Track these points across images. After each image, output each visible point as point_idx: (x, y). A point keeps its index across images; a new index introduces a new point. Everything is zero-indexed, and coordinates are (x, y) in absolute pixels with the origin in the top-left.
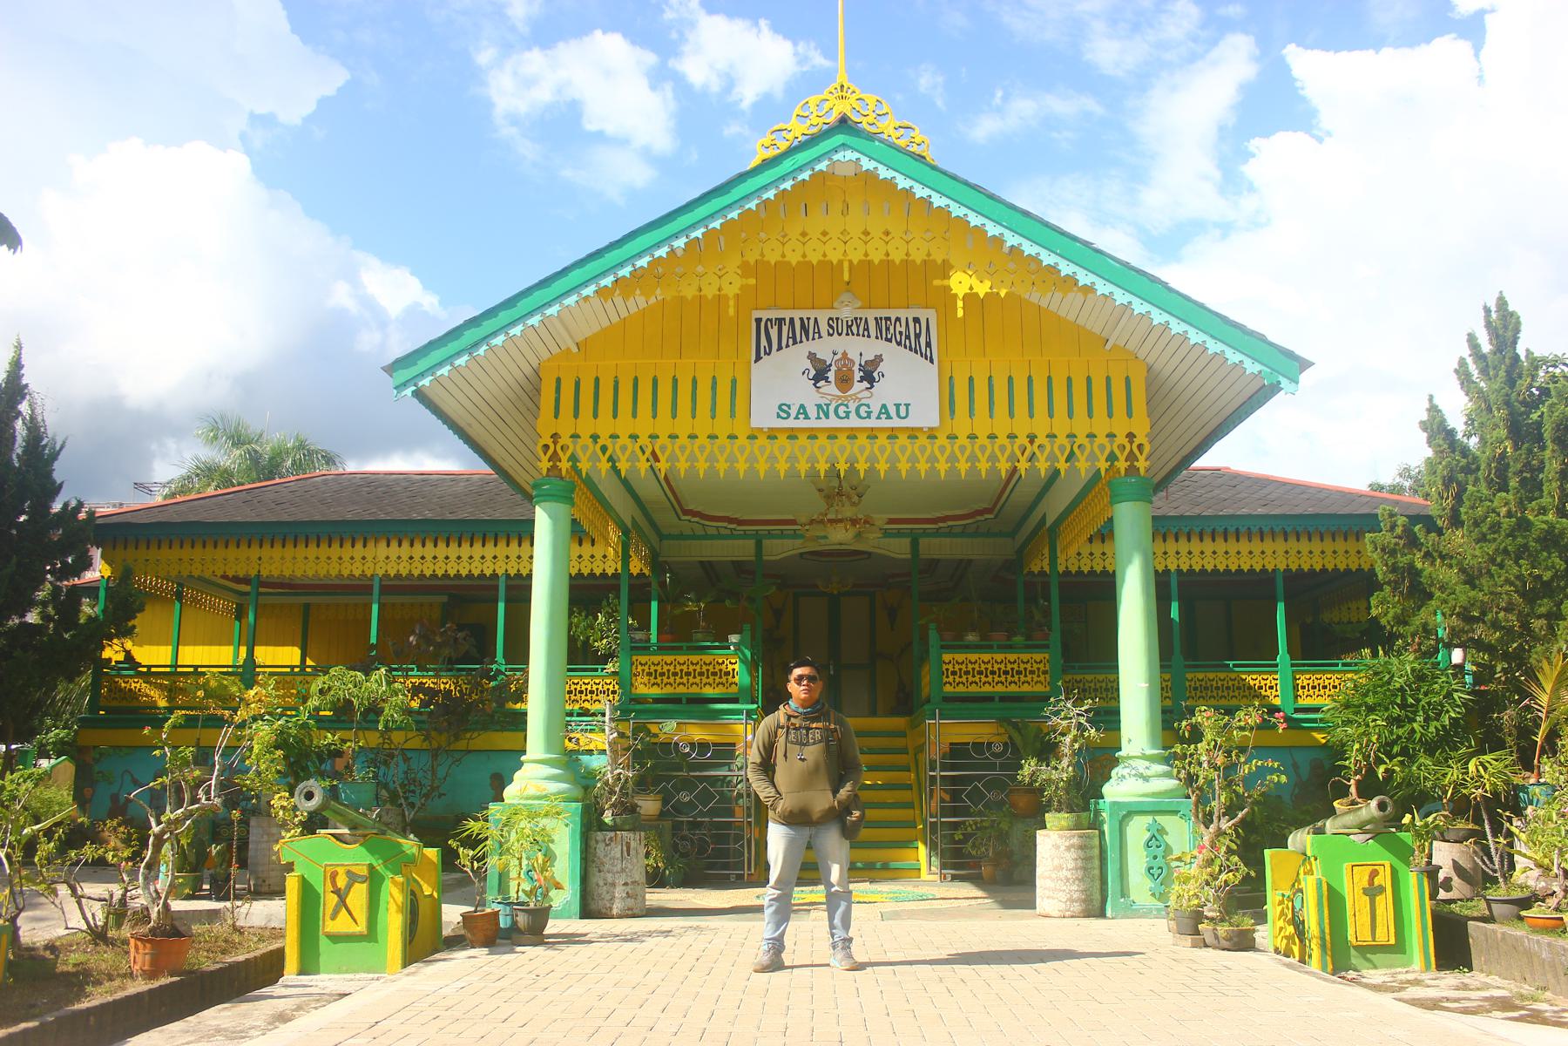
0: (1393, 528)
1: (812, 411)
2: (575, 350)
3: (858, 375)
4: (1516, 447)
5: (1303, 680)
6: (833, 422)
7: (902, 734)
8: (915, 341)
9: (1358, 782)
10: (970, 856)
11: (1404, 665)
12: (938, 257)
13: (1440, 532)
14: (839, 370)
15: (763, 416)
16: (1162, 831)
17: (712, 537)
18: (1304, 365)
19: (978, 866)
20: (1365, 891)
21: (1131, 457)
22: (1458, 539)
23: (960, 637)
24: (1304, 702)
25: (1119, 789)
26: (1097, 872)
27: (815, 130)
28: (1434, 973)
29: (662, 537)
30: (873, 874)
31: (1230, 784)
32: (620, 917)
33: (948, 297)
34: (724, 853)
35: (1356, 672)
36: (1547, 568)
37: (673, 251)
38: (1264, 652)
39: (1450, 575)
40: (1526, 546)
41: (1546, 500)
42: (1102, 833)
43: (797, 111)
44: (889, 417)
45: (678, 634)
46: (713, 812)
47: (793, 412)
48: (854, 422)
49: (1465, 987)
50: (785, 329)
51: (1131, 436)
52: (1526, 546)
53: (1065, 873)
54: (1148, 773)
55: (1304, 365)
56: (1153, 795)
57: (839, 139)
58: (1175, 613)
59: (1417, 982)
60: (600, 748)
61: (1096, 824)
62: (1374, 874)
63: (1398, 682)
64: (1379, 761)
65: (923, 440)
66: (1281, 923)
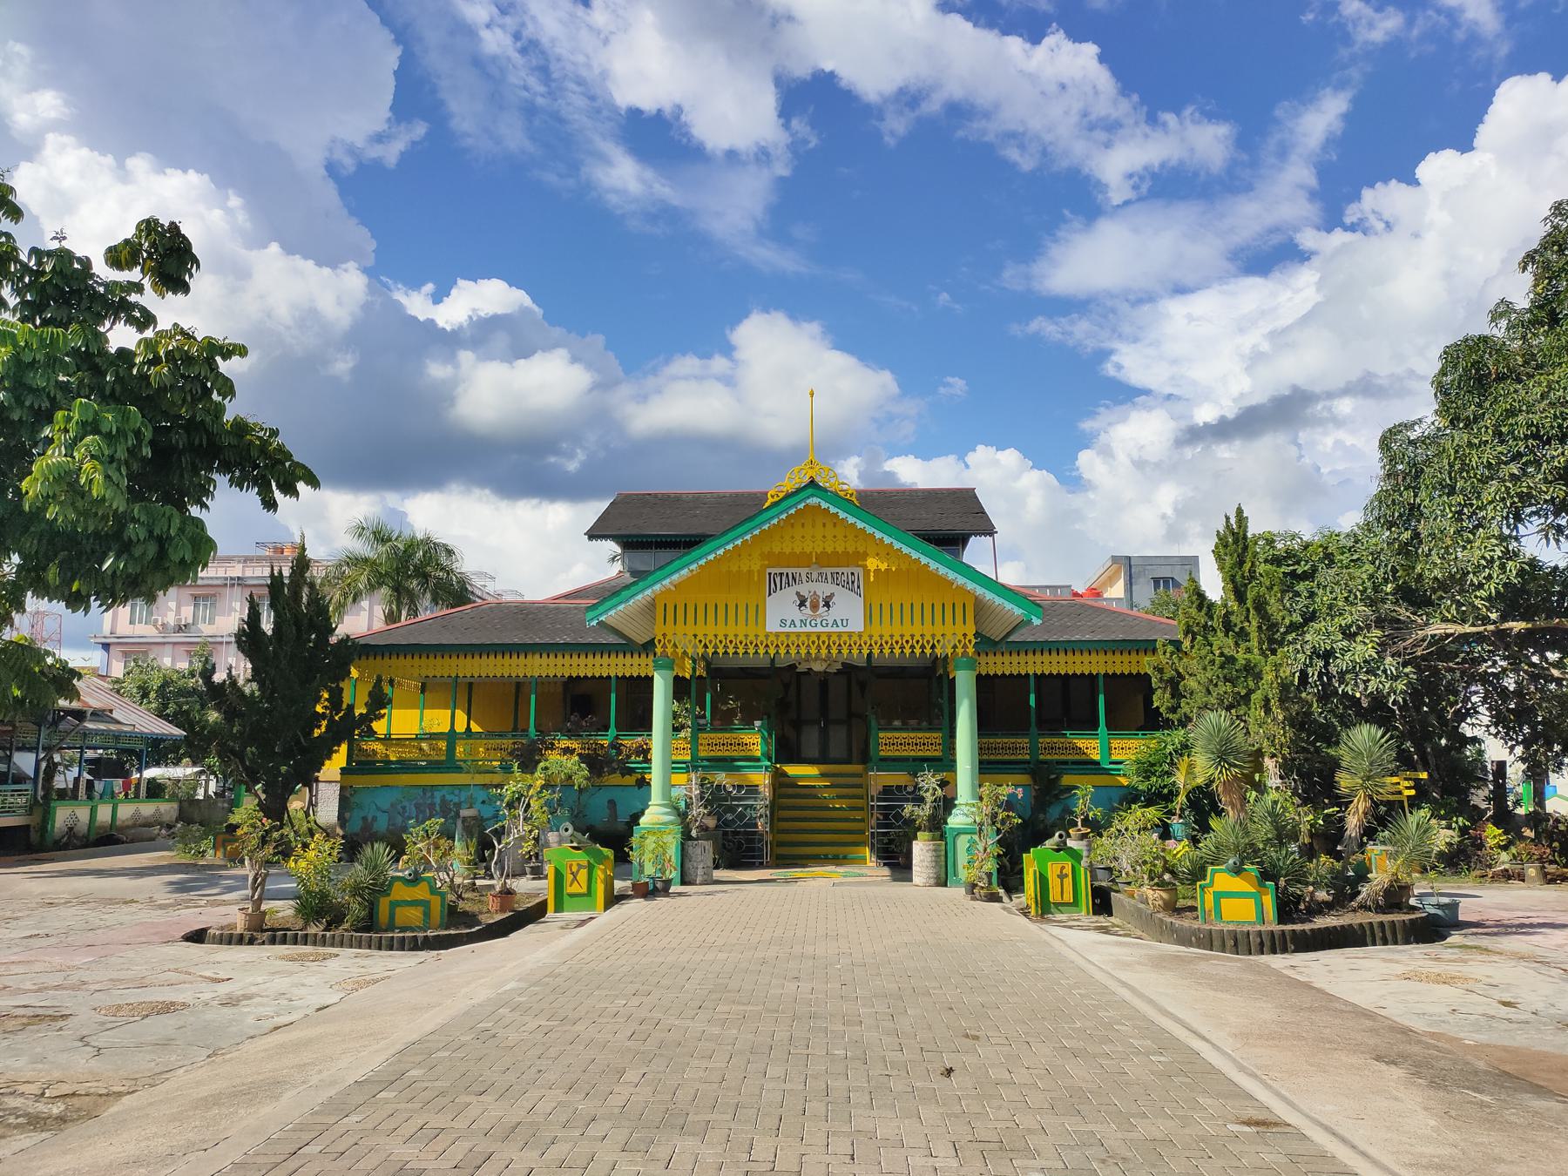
1: (798, 623)
5: (1115, 744)
6: (809, 629)
7: (860, 776)
8: (851, 586)
12: (861, 550)
15: (772, 626)
23: (890, 723)
24: (1114, 758)
25: (956, 820)
45: (723, 721)
48: (819, 629)
57: (810, 491)
60: (686, 786)
61: (942, 837)
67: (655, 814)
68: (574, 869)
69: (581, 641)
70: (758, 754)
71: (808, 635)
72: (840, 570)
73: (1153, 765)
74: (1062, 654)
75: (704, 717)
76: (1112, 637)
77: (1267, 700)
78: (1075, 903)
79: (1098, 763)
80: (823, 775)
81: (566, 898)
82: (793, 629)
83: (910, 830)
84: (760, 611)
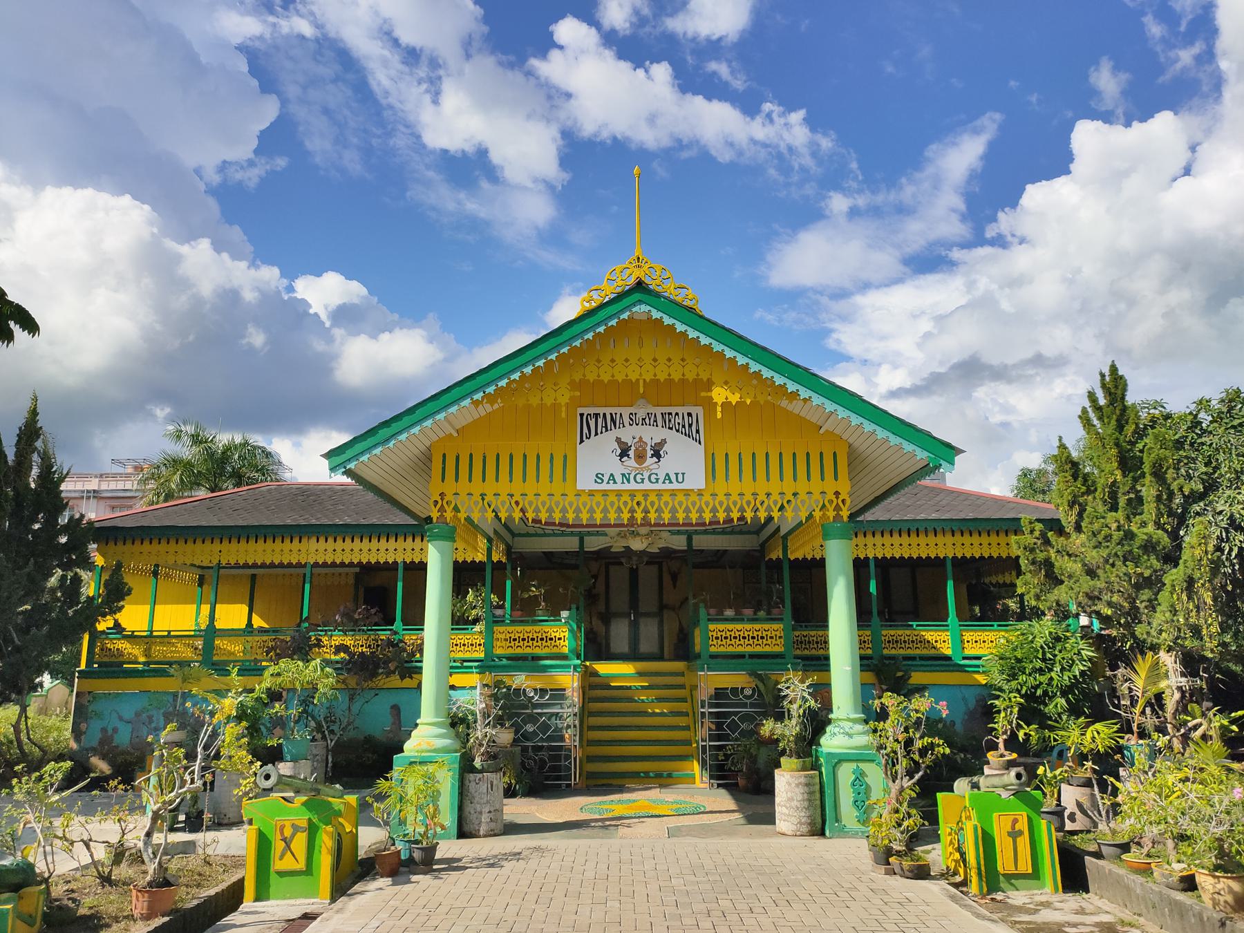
0: (1032, 532)
1: (619, 478)
2: (455, 434)
3: (650, 453)
4: (1124, 476)
5: (967, 636)
6: (633, 486)
8: (688, 429)
9: (1005, 741)
10: (730, 770)
11: (1044, 628)
12: (704, 376)
13: (1068, 536)
14: (637, 449)
15: (585, 481)
16: (863, 774)
17: (549, 535)
18: (959, 451)
19: (735, 778)
20: (1009, 834)
21: (837, 508)
22: (1078, 541)
24: (968, 652)
25: (832, 742)
26: (818, 802)
27: (619, 290)
28: (1061, 896)
29: (513, 535)
30: (662, 781)
31: (908, 753)
32: (485, 836)
33: (709, 405)
34: (555, 769)
35: (1007, 631)
36: (1147, 568)
37: (523, 375)
38: (939, 616)
39: (1075, 567)
40: (1131, 552)
41: (1145, 517)
42: (821, 773)
43: (607, 276)
44: (671, 482)
45: (526, 610)
46: (550, 738)
47: (606, 479)
48: (647, 486)
49: (1081, 911)
50: (600, 420)
51: (837, 494)
52: (1131, 552)
53: (795, 803)
54: (851, 731)
55: (959, 451)
56: (856, 748)
57: (637, 296)
58: (873, 588)
59: (1047, 905)
60: (473, 696)
61: (816, 766)
62: (1015, 821)
63: (1039, 642)
64: (1019, 727)
65: (694, 498)
66: (950, 849)
67: (426, 737)
68: (288, 832)
69: (363, 522)
70: (566, 650)
71: (632, 494)
72: (673, 410)
73: (1019, 661)
74: (905, 536)
75: (502, 607)
76: (962, 516)
77: (1190, 582)
78: (1035, 875)
79: (948, 658)
80: (641, 674)
81: (273, 878)
82: (612, 486)
83: (773, 753)
84: (568, 464)
